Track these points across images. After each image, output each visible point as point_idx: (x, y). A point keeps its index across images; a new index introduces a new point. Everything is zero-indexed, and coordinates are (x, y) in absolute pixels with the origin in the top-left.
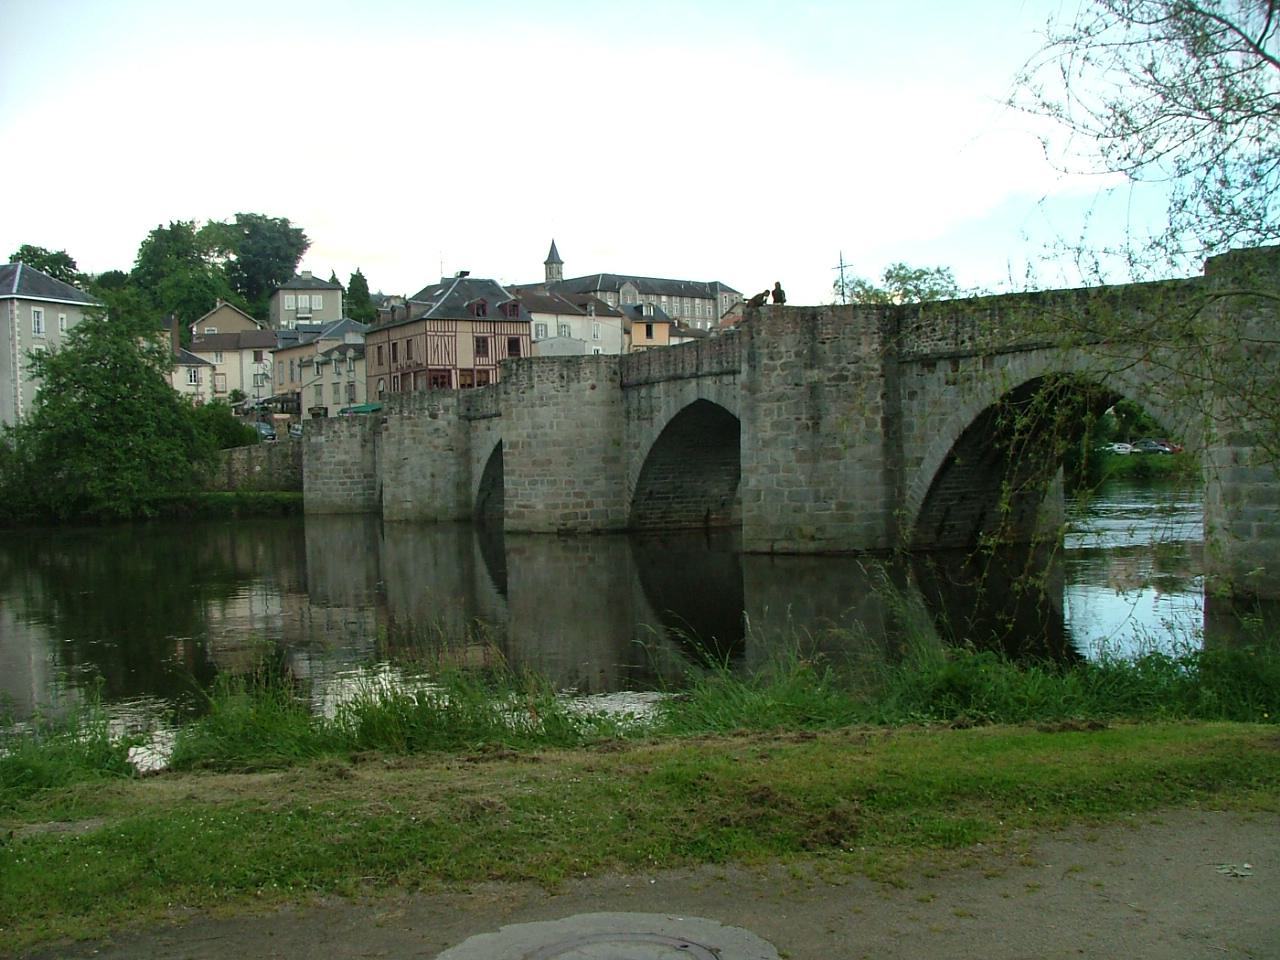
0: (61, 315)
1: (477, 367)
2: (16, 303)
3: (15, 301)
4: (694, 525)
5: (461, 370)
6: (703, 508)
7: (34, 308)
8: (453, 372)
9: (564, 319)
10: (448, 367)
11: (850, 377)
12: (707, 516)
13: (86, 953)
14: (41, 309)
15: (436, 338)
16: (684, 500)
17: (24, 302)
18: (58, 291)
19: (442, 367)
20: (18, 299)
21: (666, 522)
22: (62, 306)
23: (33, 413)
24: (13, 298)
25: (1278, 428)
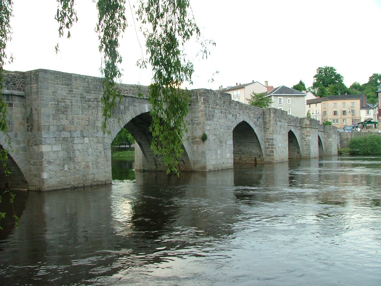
0: (288, 99)
2: (273, 97)
4: (252, 162)
6: (253, 157)
7: (279, 97)
9: (306, 102)
11: (201, 123)
12: (255, 160)
13: (228, 219)
14: (282, 98)
16: (245, 154)
17: (275, 96)
21: (242, 161)
24: (272, 96)
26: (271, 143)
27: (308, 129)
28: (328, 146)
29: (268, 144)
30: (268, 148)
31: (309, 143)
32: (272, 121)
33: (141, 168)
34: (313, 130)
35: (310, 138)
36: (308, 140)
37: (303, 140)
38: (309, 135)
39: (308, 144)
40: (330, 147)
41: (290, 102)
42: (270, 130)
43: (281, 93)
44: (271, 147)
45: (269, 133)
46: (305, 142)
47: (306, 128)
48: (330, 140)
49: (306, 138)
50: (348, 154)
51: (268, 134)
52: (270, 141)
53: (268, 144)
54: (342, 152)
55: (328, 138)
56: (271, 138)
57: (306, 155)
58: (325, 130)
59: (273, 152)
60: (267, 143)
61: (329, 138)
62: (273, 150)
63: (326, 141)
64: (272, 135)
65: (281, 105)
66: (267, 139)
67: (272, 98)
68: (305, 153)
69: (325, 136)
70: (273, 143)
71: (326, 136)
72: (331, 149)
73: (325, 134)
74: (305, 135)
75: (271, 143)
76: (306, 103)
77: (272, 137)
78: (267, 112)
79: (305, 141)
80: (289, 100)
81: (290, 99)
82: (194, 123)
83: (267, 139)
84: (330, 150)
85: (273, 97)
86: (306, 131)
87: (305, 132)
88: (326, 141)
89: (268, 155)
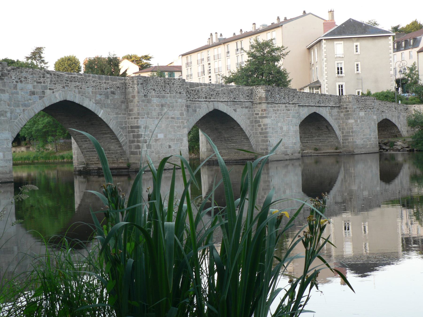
0: (355, 44)
2: (324, 41)
3: (323, 40)
20: (324, 39)
24: (322, 39)
26: (136, 133)
27: (264, 106)
28: (347, 133)
29: (133, 135)
30: (133, 142)
31: (266, 129)
32: (136, 98)
33: (354, 170)
34: (282, 107)
35: (267, 121)
36: (264, 125)
37: (257, 124)
38: (265, 115)
39: (264, 131)
41: (359, 50)
42: (134, 112)
43: (341, 34)
44: (136, 139)
45: (133, 117)
46: (260, 128)
47: (260, 103)
48: (351, 121)
49: (261, 121)
51: (132, 118)
52: (135, 130)
53: (133, 135)
56: (136, 125)
57: (263, 151)
58: (341, 104)
59: (138, 147)
60: (132, 134)
61: (349, 118)
62: (140, 144)
63: (344, 124)
64: (137, 121)
66: (131, 126)
67: (323, 44)
68: (261, 147)
69: (342, 115)
70: (140, 133)
71: (345, 115)
72: (353, 139)
73: (342, 112)
74: (260, 115)
75: (137, 133)
76: (392, 51)
77: (137, 124)
78: (130, 83)
79: (260, 126)
80: (357, 46)
81: (358, 44)
82: (318, 89)
83: (132, 127)
85: (324, 41)
86: (260, 110)
87: (259, 111)
88: (344, 124)
89: (132, 153)
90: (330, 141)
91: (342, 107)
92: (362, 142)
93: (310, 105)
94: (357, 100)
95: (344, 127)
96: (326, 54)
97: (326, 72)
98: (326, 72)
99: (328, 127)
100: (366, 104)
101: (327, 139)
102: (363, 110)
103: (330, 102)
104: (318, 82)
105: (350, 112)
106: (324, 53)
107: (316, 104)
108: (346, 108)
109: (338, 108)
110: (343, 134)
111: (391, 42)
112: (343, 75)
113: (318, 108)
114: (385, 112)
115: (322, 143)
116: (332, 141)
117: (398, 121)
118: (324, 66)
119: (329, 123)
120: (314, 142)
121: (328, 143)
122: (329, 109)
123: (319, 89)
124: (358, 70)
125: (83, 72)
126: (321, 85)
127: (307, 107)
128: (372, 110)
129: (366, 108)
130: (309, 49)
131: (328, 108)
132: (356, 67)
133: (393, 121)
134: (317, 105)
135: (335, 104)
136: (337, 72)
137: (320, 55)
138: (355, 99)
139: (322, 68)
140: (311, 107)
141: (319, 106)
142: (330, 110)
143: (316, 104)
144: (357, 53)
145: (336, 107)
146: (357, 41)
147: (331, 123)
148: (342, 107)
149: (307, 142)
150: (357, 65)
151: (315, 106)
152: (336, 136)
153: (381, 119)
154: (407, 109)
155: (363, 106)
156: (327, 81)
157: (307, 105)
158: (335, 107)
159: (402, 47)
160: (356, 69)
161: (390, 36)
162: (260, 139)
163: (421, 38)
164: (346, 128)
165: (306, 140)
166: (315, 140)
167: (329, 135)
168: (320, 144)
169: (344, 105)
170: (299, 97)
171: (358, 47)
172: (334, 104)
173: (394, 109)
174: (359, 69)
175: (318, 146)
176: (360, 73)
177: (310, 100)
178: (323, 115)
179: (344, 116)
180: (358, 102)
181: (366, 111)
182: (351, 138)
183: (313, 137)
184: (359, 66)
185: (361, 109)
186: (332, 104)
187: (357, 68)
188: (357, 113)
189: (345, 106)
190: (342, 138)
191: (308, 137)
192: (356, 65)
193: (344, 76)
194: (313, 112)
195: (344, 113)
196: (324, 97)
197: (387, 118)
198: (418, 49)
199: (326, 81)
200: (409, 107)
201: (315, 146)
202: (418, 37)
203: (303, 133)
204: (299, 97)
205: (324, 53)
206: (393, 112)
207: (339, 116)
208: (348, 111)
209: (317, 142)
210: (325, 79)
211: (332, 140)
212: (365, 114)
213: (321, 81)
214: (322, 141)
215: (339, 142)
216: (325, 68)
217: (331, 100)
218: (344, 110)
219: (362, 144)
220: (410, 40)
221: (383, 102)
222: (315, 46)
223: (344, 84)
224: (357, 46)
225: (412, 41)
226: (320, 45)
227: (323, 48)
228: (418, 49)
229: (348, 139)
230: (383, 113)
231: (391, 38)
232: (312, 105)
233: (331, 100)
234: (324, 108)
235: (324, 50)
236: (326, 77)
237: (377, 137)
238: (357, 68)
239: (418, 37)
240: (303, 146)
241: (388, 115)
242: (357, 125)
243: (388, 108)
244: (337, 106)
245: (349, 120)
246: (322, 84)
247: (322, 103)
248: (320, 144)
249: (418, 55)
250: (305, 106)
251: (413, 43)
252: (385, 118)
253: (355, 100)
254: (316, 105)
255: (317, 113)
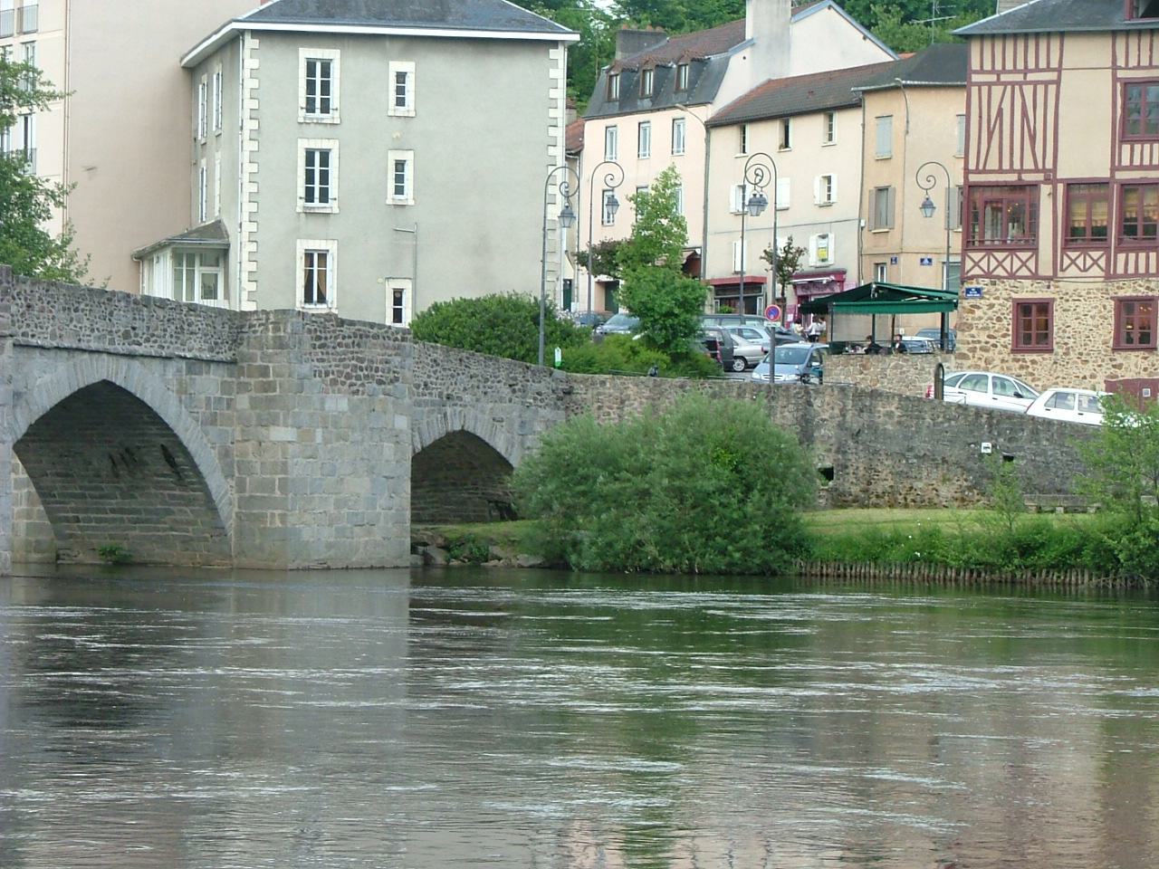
0: (396, 66)
1: (1120, 175)
2: (250, 43)
3: (248, 38)
5: (1071, 185)
7: (307, 52)
8: (1045, 189)
10: (1027, 178)
14: (332, 54)
15: (997, 90)
18: (574, 21)
19: (1012, 178)
20: (255, 33)
22: (397, 46)
23: (68, 359)
24: (242, 32)
25: (416, 867)
40: (278, 493)
41: (409, 97)
43: (329, 17)
48: (281, 433)
50: (525, 559)
54: (495, 550)
55: (264, 424)
58: (243, 349)
61: (275, 422)
63: (250, 446)
65: (327, 118)
69: (243, 402)
71: (254, 403)
72: (283, 518)
73: (243, 388)
80: (401, 77)
81: (407, 66)
84: (278, 524)
85: (250, 43)
88: (250, 446)
90: (181, 522)
91: (245, 364)
92: (328, 534)
93: (83, 345)
94: (319, 338)
95: (251, 457)
96: (255, 104)
97: (254, 188)
98: (254, 188)
99: (175, 459)
100: (358, 359)
101: (169, 512)
102: (343, 383)
103: (184, 337)
104: (217, 229)
105: (278, 392)
106: (247, 94)
107: (112, 342)
108: (264, 372)
109: (222, 370)
110: (244, 491)
111: (559, 73)
112: (333, 206)
113: (123, 361)
114: (460, 399)
115: (148, 530)
116: (188, 523)
117: (522, 443)
118: (246, 160)
119: (175, 436)
120: (106, 520)
121: (172, 529)
122: (179, 371)
123: (221, 264)
124: (399, 190)
125: (314, 8)
126: (229, 245)
127: (65, 354)
128: (391, 387)
129: (358, 378)
130: (194, 70)
131: (172, 367)
132: (392, 174)
133: (500, 445)
134: (120, 349)
135: (211, 350)
136: (302, 192)
137: (231, 104)
138: (310, 331)
139: (234, 168)
140: (86, 356)
141: (131, 356)
142: (186, 378)
143: (112, 342)
144: (401, 111)
145: (219, 362)
146: (402, 56)
147: (185, 438)
148: (245, 364)
149: (77, 520)
150: (400, 165)
151: (109, 353)
152: (208, 494)
153: (433, 433)
154: (568, 393)
155: (346, 366)
156: (253, 227)
157: (66, 345)
158: (209, 362)
159: (643, 97)
160: (391, 184)
161: (554, 44)
162: (540, 366)
163: (725, 65)
164: (258, 466)
165: (73, 510)
166: (113, 511)
167: (177, 492)
168: (137, 532)
169: (252, 358)
170: (29, 306)
171: (410, 85)
172: (206, 346)
173: (506, 391)
174: (408, 185)
175: (126, 538)
176: (411, 202)
177: (87, 324)
178: (147, 399)
179: (252, 407)
180: (322, 346)
181: (357, 392)
182: (277, 512)
183: (102, 497)
184: (408, 172)
185: (334, 382)
186: (196, 347)
187: (399, 179)
188: (316, 398)
189: (259, 363)
190: (236, 509)
191: (83, 496)
192: (392, 166)
193: (336, 210)
194: (95, 378)
195: (253, 394)
196: (161, 313)
197: (470, 427)
198: (707, 112)
199: (249, 227)
200: (576, 386)
201: (111, 537)
202: (713, 58)
203: (58, 475)
204: (29, 306)
205: (247, 94)
206: (501, 400)
207: (229, 407)
208: (268, 387)
209: (122, 520)
210: (246, 217)
211: (191, 517)
212: (353, 408)
213: (229, 225)
214: (143, 516)
215: (220, 530)
216: (250, 167)
217: (193, 328)
218: (252, 381)
219: (329, 546)
220: (680, 67)
221: (454, 354)
222: (218, 58)
223: (332, 247)
224: (401, 77)
225: (685, 73)
226: (236, 53)
227: (247, 73)
228: (707, 112)
229: (261, 518)
230: (448, 403)
231: (560, 55)
232: (94, 345)
233: (193, 328)
234: (156, 363)
235: (250, 84)
236: (249, 208)
237: (408, 514)
238: (399, 179)
239: (713, 58)
240: (60, 536)
241: (471, 412)
242: (309, 453)
243: (474, 382)
244: (221, 357)
245: (272, 428)
246: (232, 240)
247: (147, 340)
248: (137, 532)
249: (708, 141)
250: (57, 348)
251: (692, 83)
252: (458, 428)
253: (307, 336)
254: (111, 348)
255: (120, 388)
